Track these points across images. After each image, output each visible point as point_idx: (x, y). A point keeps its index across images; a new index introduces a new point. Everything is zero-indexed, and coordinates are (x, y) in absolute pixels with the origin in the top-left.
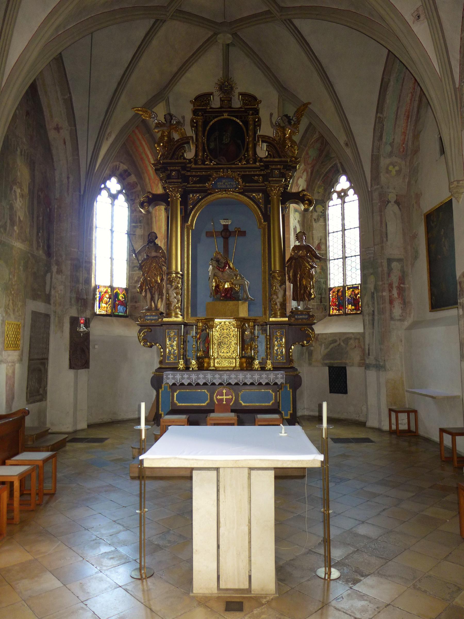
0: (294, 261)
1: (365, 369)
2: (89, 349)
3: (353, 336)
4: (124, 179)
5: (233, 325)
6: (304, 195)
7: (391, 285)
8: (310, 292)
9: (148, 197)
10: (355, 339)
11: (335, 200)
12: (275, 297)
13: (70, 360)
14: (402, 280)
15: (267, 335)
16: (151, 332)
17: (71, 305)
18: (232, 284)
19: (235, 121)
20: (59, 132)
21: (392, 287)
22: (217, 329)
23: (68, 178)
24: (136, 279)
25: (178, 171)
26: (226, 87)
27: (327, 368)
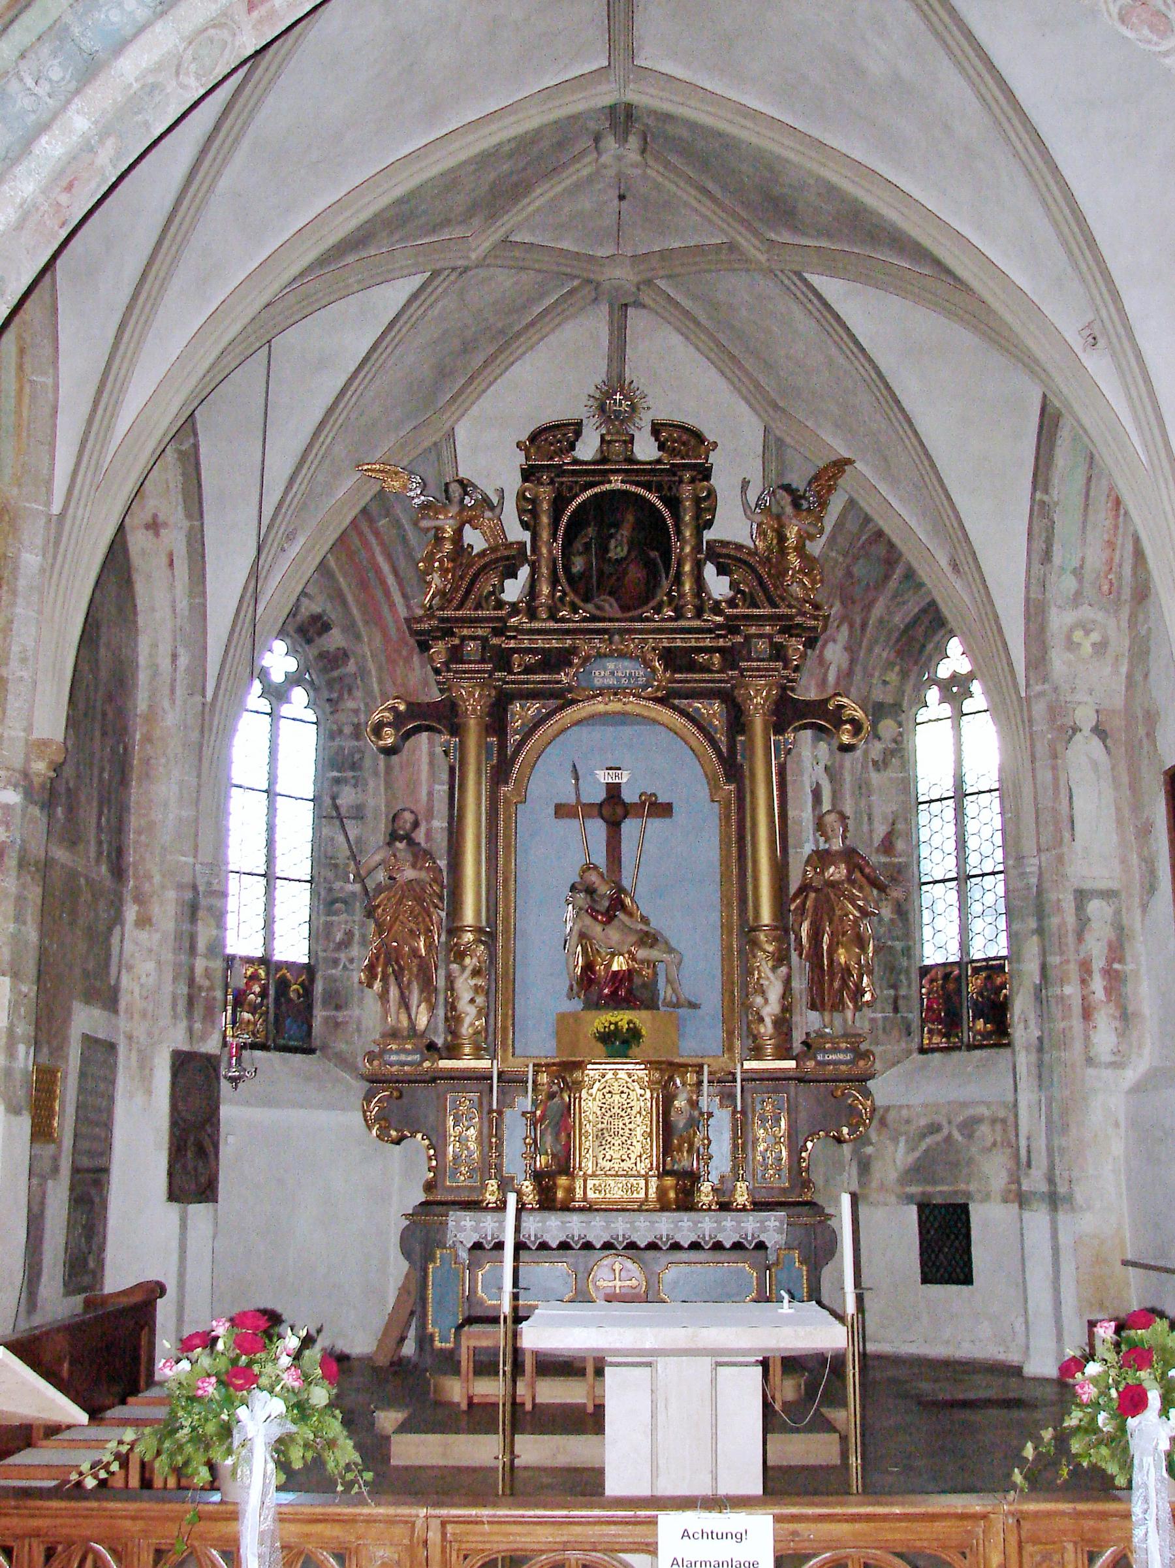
0: (812, 895)
1: (1021, 1207)
2: (216, 1146)
3: (987, 1113)
4: (309, 641)
5: (639, 1081)
6: (841, 707)
7: (1085, 967)
8: (858, 985)
9: (393, 709)
10: (994, 1121)
11: (934, 704)
12: (759, 1000)
13: (170, 1174)
14: (1117, 951)
15: (734, 1112)
16: (400, 1097)
17: (175, 1016)
18: (634, 959)
19: (643, 498)
20: (157, 535)
21: (1089, 972)
22: (594, 1091)
23: (174, 657)
24: (339, 937)
25: (484, 640)
26: (615, 402)
27: (915, 1208)
